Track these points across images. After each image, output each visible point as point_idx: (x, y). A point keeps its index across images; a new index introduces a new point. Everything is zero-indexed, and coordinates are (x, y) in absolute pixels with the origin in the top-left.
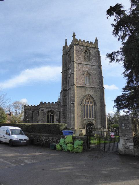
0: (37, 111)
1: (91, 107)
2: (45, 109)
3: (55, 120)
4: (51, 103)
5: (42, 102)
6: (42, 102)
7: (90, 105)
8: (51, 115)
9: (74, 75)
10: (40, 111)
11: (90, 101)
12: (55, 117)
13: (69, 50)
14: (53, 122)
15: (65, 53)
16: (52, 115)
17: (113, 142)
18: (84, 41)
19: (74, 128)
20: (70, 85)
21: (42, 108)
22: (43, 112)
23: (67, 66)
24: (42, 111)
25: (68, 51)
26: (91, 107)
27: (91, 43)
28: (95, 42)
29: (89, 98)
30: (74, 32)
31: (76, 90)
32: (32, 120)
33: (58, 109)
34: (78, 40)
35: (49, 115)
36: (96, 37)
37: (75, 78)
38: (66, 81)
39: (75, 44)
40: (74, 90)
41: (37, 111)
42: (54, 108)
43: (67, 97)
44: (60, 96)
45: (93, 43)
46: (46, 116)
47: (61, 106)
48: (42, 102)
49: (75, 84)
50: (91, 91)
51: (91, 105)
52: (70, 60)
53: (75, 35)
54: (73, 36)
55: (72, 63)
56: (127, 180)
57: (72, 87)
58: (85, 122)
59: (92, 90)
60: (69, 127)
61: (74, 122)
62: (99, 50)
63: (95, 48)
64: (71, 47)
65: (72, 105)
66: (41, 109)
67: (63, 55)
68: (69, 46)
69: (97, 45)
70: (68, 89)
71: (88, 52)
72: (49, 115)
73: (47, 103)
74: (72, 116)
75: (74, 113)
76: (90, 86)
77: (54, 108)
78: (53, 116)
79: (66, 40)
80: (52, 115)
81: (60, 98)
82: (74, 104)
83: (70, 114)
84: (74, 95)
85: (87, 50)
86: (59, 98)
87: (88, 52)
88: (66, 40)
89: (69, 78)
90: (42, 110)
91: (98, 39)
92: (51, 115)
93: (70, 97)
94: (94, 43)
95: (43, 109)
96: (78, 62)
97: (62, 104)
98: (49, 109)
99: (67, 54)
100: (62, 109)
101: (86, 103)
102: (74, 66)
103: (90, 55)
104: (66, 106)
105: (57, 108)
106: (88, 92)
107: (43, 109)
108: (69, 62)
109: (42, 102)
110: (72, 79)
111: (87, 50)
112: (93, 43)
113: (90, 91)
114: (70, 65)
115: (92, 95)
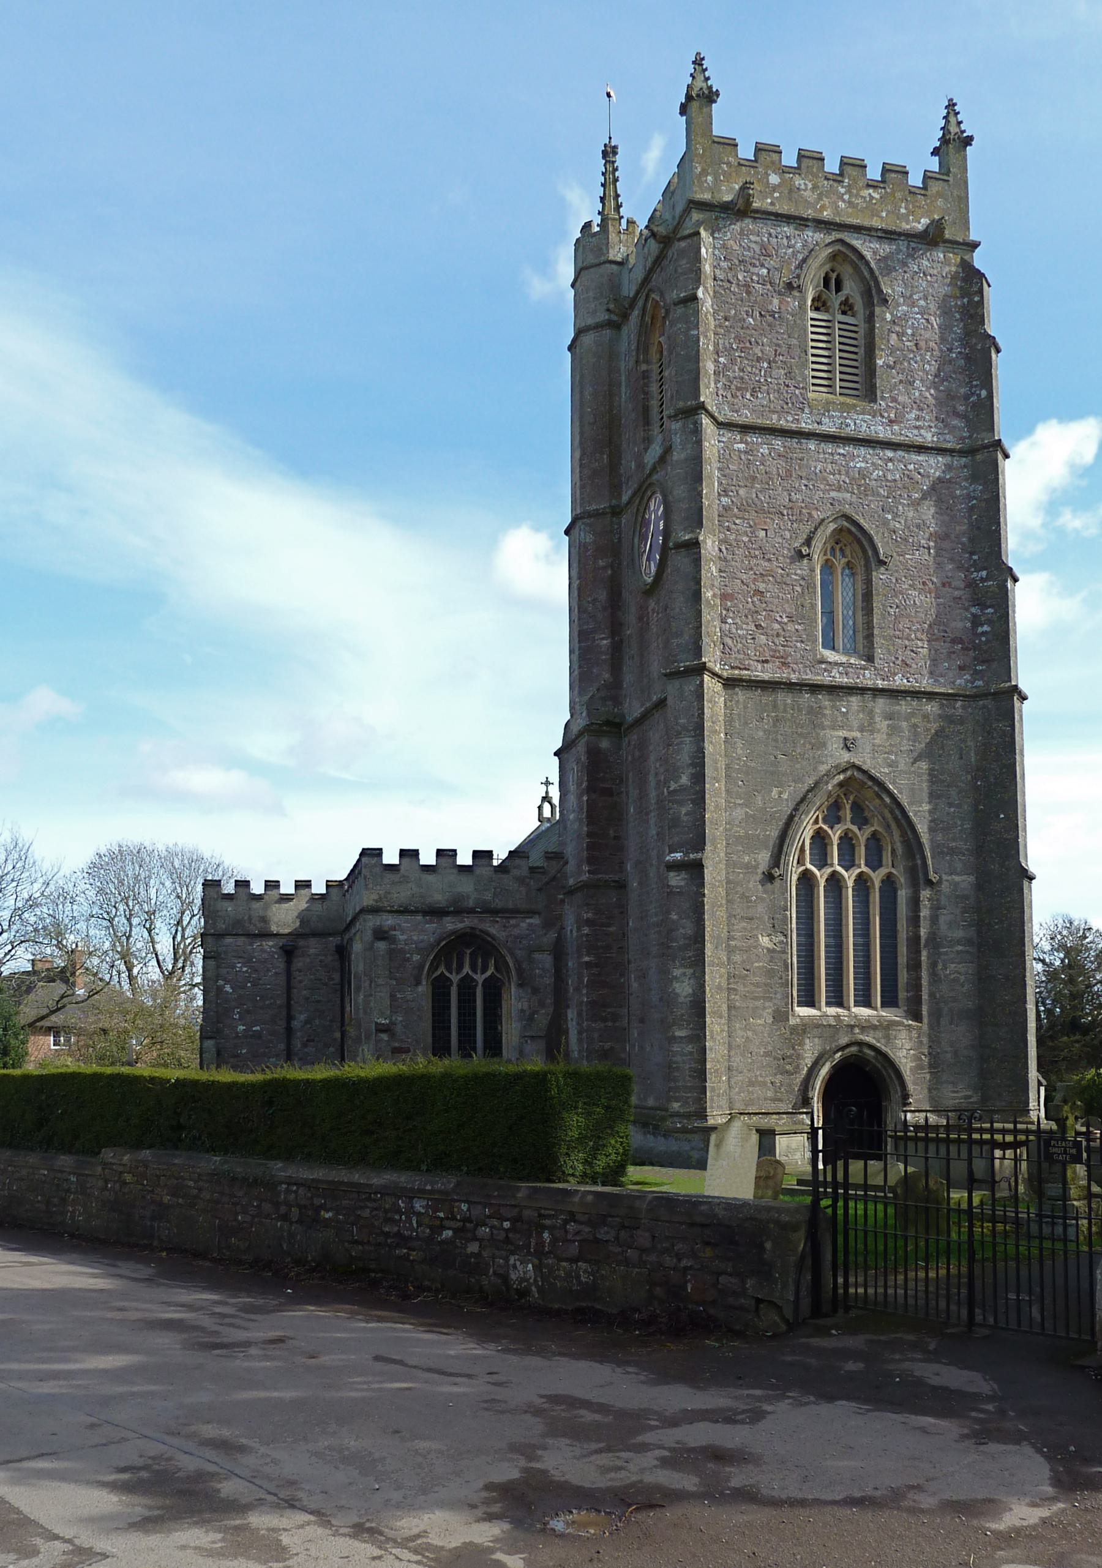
0: (333, 941)
1: (876, 898)
2: (404, 921)
3: (511, 1031)
4: (428, 858)
5: (378, 852)
6: (371, 855)
7: (835, 880)
8: (467, 985)
9: (697, 562)
10: (357, 947)
11: (862, 836)
12: (514, 1001)
13: (646, 280)
14: (494, 1047)
15: (603, 316)
16: (480, 978)
17: (1034, 1228)
18: (810, 159)
19: (702, 1115)
20: (656, 668)
21: (375, 910)
22: (392, 954)
23: (628, 464)
24: (382, 946)
25: (629, 289)
26: (876, 898)
27: (893, 173)
28: (934, 164)
29: (857, 808)
30: (698, 62)
31: (720, 727)
32: (289, 1030)
33: (535, 921)
34: (746, 152)
35: (455, 978)
36: (951, 105)
37: (707, 594)
38: (616, 628)
39: (702, 206)
40: (700, 727)
41: (333, 941)
42: (495, 912)
43: (634, 793)
44: (555, 778)
45: (915, 180)
46: (424, 988)
47: (571, 892)
48: (378, 852)
49: (712, 657)
50: (883, 725)
51: (877, 878)
52: (654, 388)
53: (710, 97)
54: (684, 110)
55: (676, 426)
56: (759, 1421)
57: (672, 688)
58: (809, 1051)
59: (889, 717)
60: (651, 1102)
61: (703, 1050)
62: (979, 260)
63: (932, 238)
64: (666, 241)
65: (676, 880)
66: (371, 922)
67: (579, 333)
68: (642, 223)
69: (963, 201)
70: (633, 709)
71: (851, 288)
72: (455, 978)
73: (391, 857)
74: (683, 989)
75: (698, 963)
76: (868, 678)
77: (495, 912)
78: (494, 993)
79: (609, 152)
80: (480, 978)
81: (556, 801)
82: (697, 868)
83: (664, 972)
84: (699, 778)
85: (846, 271)
86: (546, 798)
87: (851, 288)
88: (609, 152)
89: (652, 590)
90: (381, 934)
91: (969, 129)
92: (467, 985)
93: (660, 801)
94: (927, 177)
95: (389, 921)
96: (747, 416)
97: (577, 872)
98: (451, 924)
99: (625, 316)
100: (580, 923)
101: (822, 861)
102: (696, 461)
103: (870, 319)
104: (621, 886)
105: (532, 913)
106: (848, 745)
107: (389, 921)
108: (646, 410)
109: (371, 855)
110: (679, 604)
111: (846, 271)
112: (915, 180)
113: (868, 727)
114: (655, 451)
115: (881, 772)
